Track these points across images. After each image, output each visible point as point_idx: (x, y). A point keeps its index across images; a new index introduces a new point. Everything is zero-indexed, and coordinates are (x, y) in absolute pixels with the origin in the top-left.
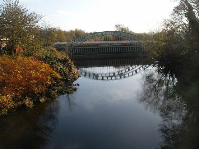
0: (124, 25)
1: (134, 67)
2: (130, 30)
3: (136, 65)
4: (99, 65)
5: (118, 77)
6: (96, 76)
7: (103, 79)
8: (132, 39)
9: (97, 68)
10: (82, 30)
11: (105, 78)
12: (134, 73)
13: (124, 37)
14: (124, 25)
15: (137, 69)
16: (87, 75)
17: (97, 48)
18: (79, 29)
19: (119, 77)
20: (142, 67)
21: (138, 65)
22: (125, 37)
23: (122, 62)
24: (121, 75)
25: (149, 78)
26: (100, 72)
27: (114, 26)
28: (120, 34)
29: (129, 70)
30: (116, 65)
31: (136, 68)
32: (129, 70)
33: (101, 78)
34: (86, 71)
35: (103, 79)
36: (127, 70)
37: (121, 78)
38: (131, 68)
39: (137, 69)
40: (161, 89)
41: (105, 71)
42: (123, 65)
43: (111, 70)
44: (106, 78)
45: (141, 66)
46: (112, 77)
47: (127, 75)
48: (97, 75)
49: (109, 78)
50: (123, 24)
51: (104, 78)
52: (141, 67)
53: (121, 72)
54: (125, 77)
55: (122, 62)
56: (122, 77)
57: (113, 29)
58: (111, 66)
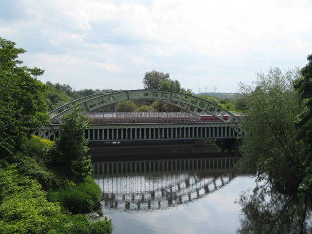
0: (168, 75)
3: (226, 176)
5: (164, 203)
7: (128, 206)
8: (196, 109)
11: (133, 206)
12: (202, 192)
13: (177, 103)
14: (168, 75)
20: (214, 181)
21: (202, 176)
22: (179, 104)
23: (212, 164)
24: (172, 198)
25: (251, 209)
29: (188, 185)
30: (152, 172)
31: (198, 185)
32: (188, 185)
33: (122, 205)
35: (128, 206)
36: (183, 185)
37: (170, 203)
38: (192, 181)
40: (306, 229)
42: (172, 175)
43: (139, 185)
45: (211, 180)
47: (185, 198)
48: (113, 196)
49: (145, 205)
50: (165, 73)
54: (180, 203)
55: (212, 164)
56: (174, 202)
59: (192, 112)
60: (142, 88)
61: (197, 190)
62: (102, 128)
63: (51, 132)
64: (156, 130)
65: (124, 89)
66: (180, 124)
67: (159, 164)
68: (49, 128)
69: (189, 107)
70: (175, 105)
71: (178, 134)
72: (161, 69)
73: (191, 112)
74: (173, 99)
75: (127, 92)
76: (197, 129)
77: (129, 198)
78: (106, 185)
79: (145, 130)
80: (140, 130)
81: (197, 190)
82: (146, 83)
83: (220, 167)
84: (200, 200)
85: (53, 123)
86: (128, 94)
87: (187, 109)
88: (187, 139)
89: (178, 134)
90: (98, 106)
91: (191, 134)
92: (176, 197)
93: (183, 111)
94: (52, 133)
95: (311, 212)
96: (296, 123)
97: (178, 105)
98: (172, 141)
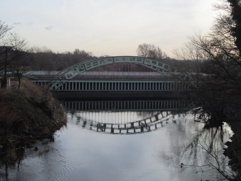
1: (164, 114)
2: (85, 52)
4: (117, 108)
6: (102, 127)
7: (112, 132)
9: (114, 113)
10: (86, 51)
13: (150, 66)
15: (155, 121)
16: (88, 126)
17: (164, 84)
18: (81, 50)
19: (139, 130)
22: (152, 67)
24: (143, 127)
26: (103, 121)
27: (137, 47)
28: (142, 61)
31: (162, 120)
32: (157, 119)
34: (86, 119)
35: (112, 132)
36: (153, 119)
37: (142, 131)
38: (160, 116)
39: (155, 121)
41: (132, 116)
44: (126, 131)
46: (128, 129)
47: (152, 128)
48: (105, 125)
49: (132, 131)
51: (115, 131)
52: (147, 119)
53: (144, 122)
56: (145, 130)
57: (134, 53)
58: (134, 111)
60: (136, 55)
62: (96, 82)
63: (60, 84)
64: (100, 84)
66: (115, 80)
67: (174, 103)
68: (59, 81)
70: (149, 67)
72: (142, 43)
73: (160, 72)
74: (146, 63)
75: (113, 57)
76: (153, 84)
77: (159, 126)
78: (97, 117)
79: (125, 84)
80: (112, 84)
82: (74, 53)
83: (133, 107)
84: (134, 135)
85: (61, 78)
86: (113, 59)
87: (157, 70)
88: (167, 90)
90: (93, 67)
91: (139, 87)
92: (147, 126)
93: (155, 71)
94: (61, 85)
97: (151, 67)
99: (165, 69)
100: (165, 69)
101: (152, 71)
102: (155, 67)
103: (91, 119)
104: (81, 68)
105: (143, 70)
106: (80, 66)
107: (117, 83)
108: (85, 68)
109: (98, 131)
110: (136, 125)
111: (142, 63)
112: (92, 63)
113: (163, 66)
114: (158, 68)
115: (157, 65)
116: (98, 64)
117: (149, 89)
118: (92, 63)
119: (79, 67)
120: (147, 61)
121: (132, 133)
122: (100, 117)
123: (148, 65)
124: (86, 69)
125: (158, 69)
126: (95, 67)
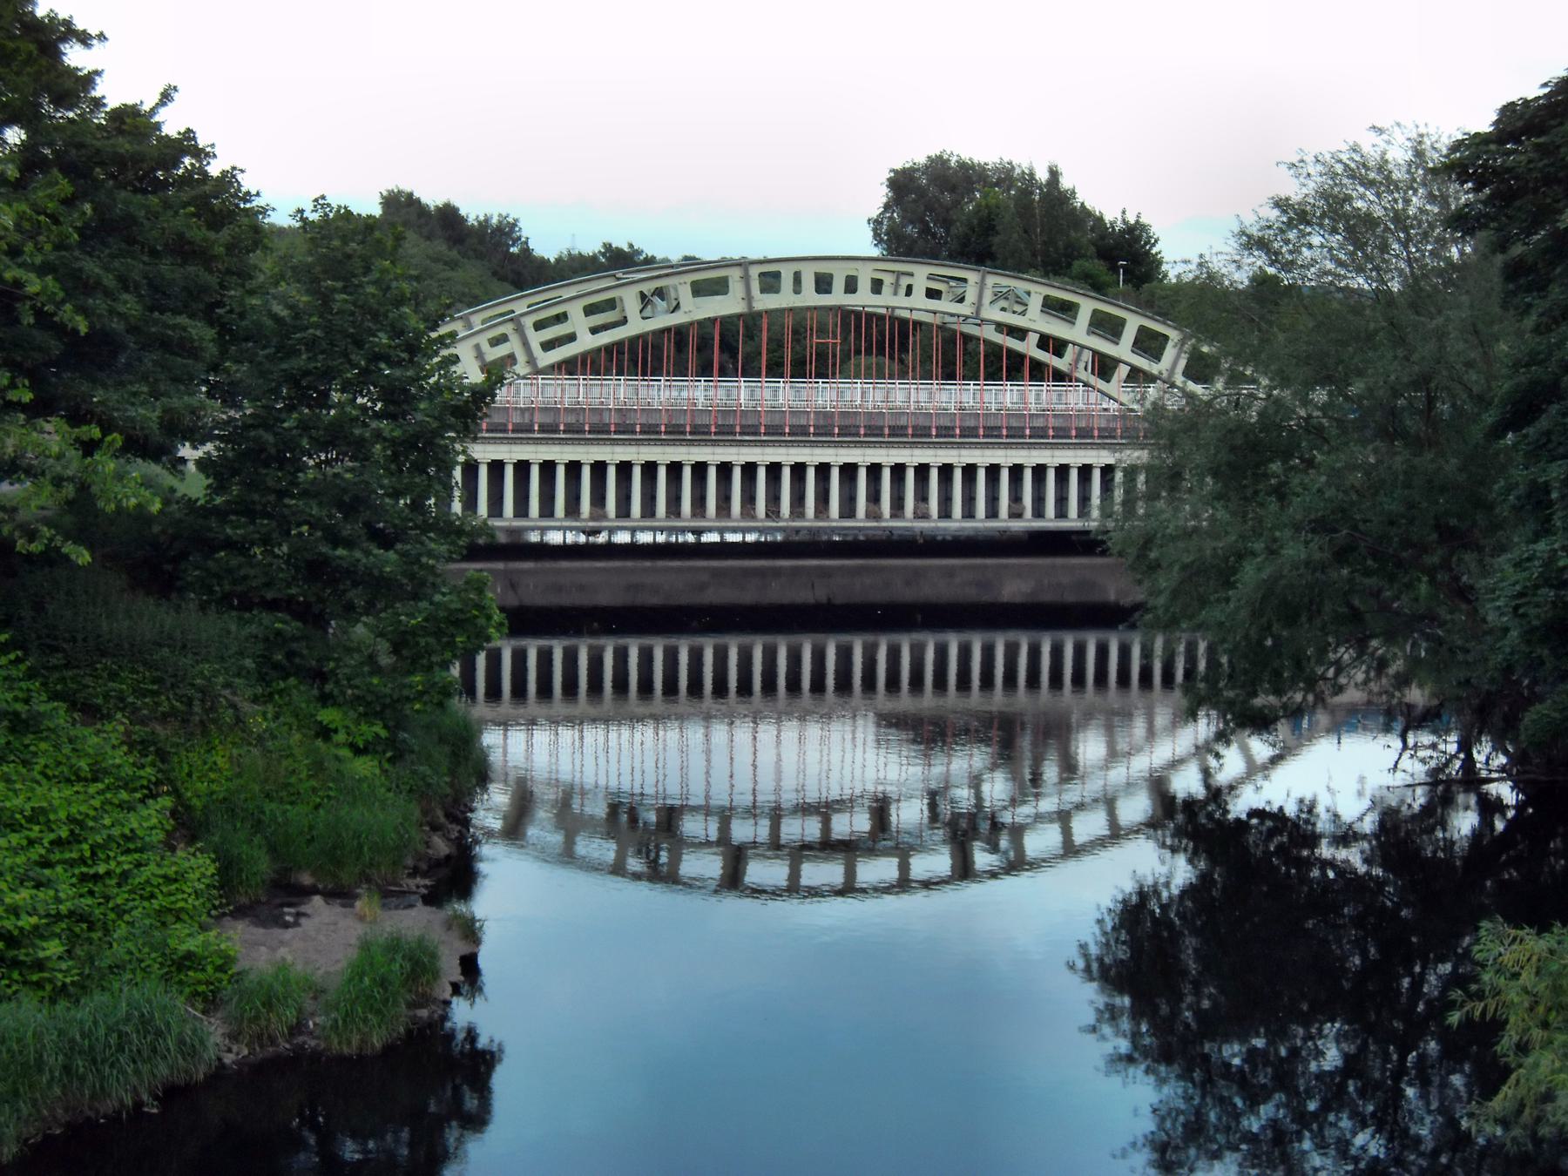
8: (1123, 371)
11: (765, 871)
13: (1019, 333)
31: (1118, 774)
33: (705, 865)
46: (848, 849)
48: (670, 816)
54: (1017, 864)
59: (1101, 384)
61: (1063, 817)
65: (736, 255)
69: (1087, 355)
71: (1016, 497)
73: (1093, 380)
81: (1063, 817)
84: (1071, 867)
89: (1016, 497)
90: (587, 342)
92: (996, 827)
93: (1059, 376)
95: (1281, 1173)
96: (1513, 507)
97: (1029, 348)
98: (608, 631)
99: (1142, 362)
100: (1142, 362)
101: (1038, 372)
102: (1056, 346)
103: (566, 772)
104: (485, 347)
105: (858, 327)
106: (483, 340)
107: (725, 469)
108: (526, 344)
109: (618, 869)
110: (909, 814)
111: (965, 309)
112: (575, 311)
113: (1129, 334)
114: (1083, 347)
115: (1123, 350)
116: (624, 321)
117: (921, 515)
118: (575, 311)
119: (474, 341)
120: (998, 296)
121: (775, 893)
122: (813, 756)
123: (1000, 327)
124: (531, 361)
125: (1080, 354)
126: (606, 338)
